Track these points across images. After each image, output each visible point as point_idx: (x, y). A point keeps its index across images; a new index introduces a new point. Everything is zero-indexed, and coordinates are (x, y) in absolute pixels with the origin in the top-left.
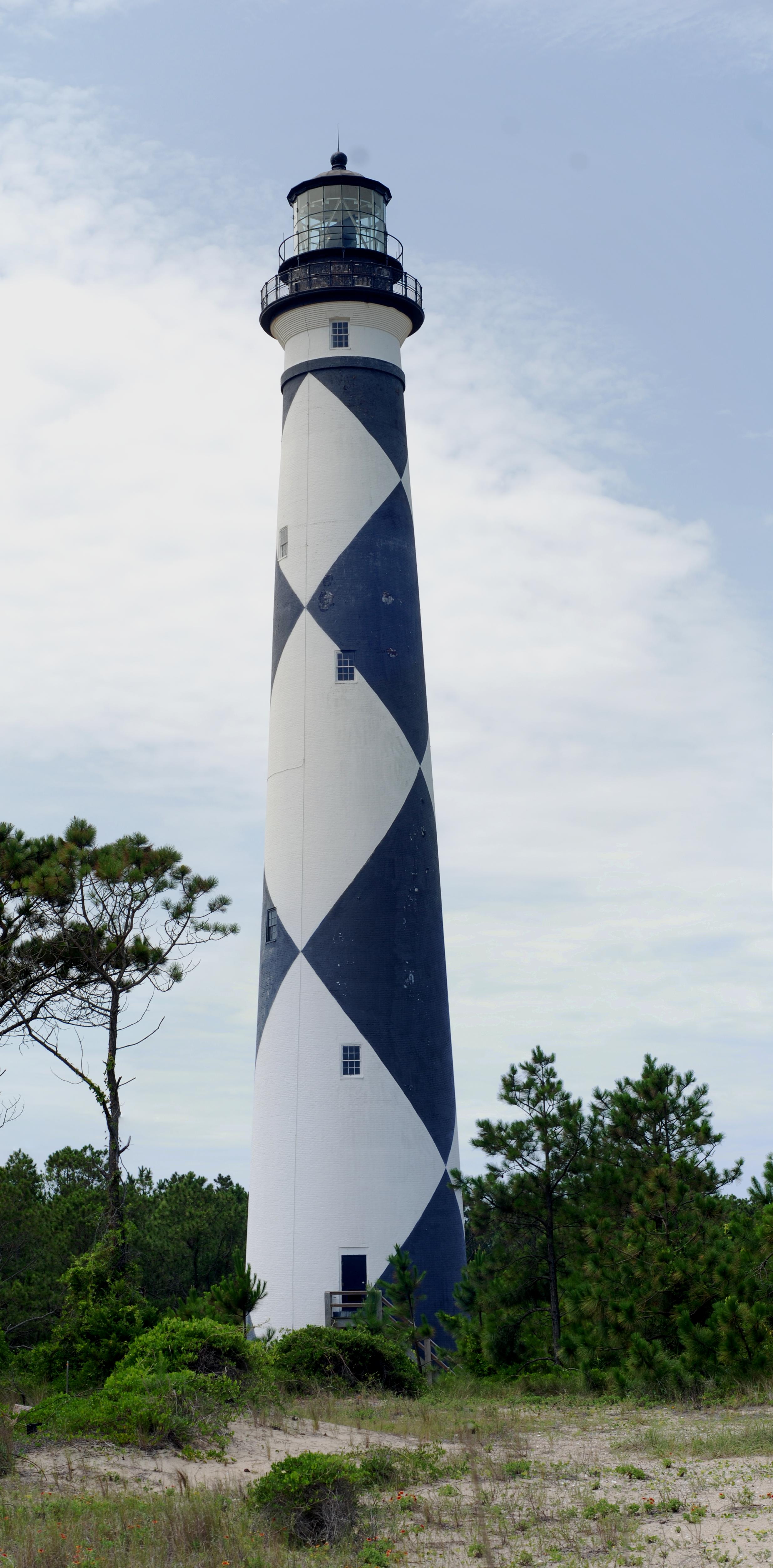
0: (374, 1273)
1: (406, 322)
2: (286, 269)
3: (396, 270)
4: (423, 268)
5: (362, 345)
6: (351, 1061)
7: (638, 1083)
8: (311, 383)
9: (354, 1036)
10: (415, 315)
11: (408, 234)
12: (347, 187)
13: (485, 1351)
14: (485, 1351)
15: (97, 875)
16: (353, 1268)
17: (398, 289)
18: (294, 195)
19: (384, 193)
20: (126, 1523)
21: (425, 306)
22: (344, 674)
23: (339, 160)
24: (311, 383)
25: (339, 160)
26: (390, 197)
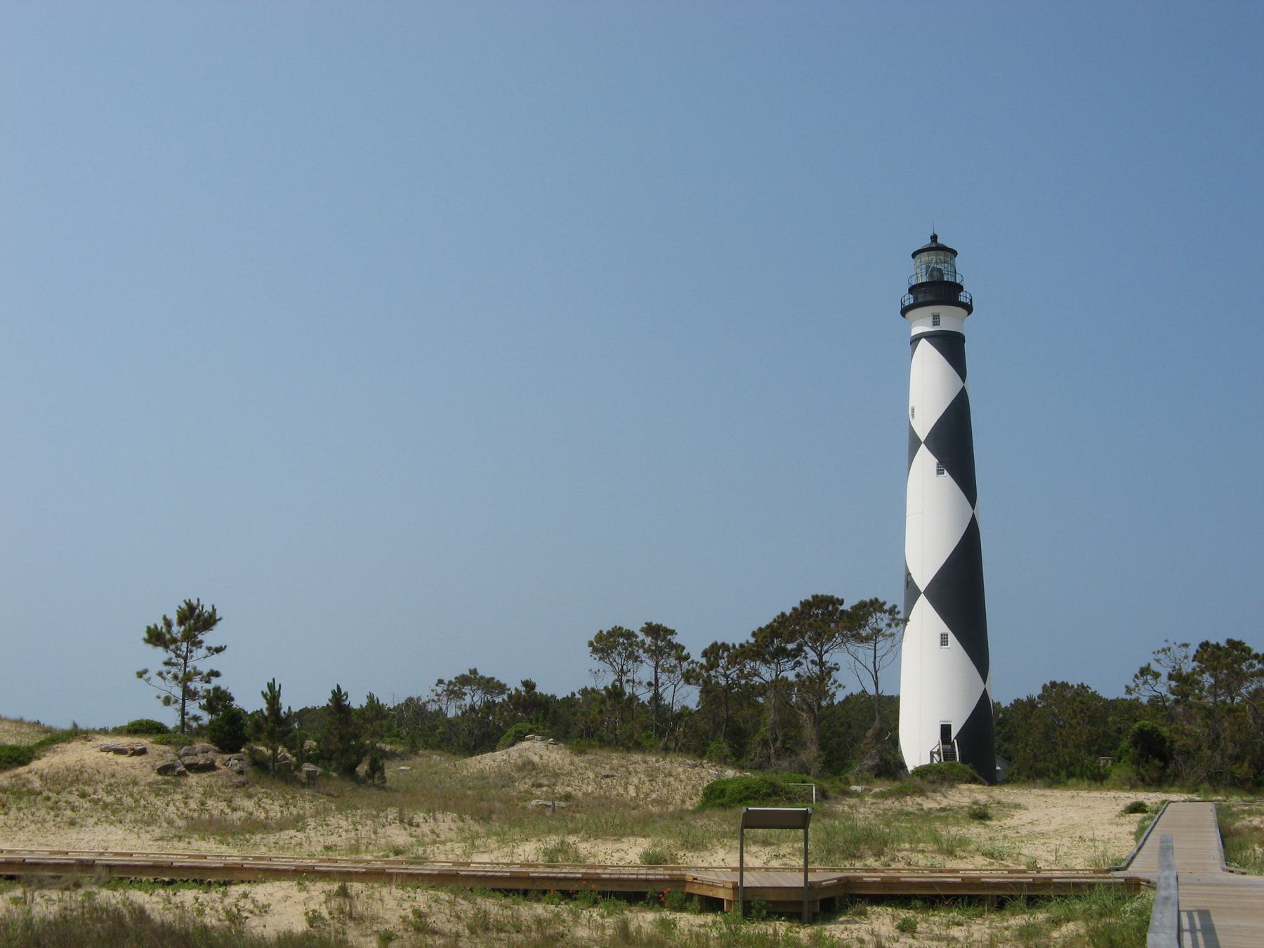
0: (954, 733)
1: (965, 312)
2: (912, 290)
3: (960, 288)
4: (971, 289)
5: (946, 325)
6: (944, 640)
7: (994, 697)
8: (924, 342)
9: (944, 628)
10: (968, 308)
11: (965, 271)
12: (936, 247)
13: (1137, 725)
14: (1137, 725)
15: (1079, 936)
16: (946, 730)
17: (962, 299)
18: (914, 255)
19: (954, 253)
20: (762, 938)
22: (939, 472)
23: (934, 238)
24: (924, 342)
25: (934, 238)
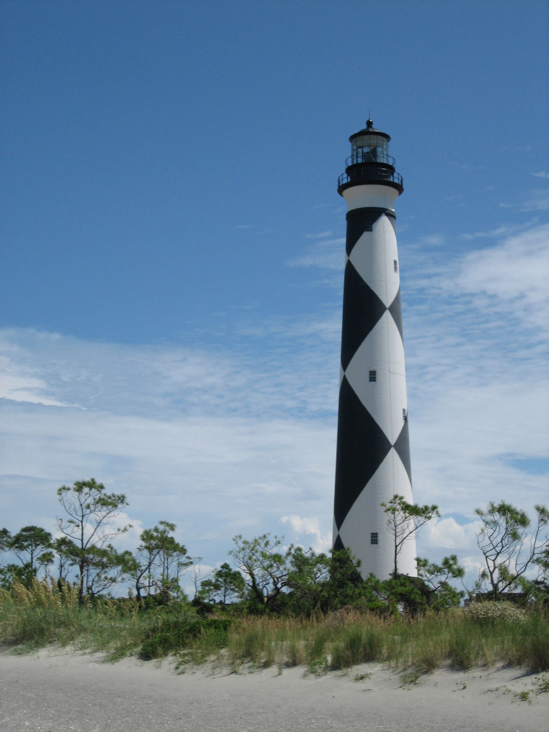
18: (353, 138)
19: (387, 137)
21: (404, 186)
23: (369, 124)
25: (369, 124)
26: (390, 138)
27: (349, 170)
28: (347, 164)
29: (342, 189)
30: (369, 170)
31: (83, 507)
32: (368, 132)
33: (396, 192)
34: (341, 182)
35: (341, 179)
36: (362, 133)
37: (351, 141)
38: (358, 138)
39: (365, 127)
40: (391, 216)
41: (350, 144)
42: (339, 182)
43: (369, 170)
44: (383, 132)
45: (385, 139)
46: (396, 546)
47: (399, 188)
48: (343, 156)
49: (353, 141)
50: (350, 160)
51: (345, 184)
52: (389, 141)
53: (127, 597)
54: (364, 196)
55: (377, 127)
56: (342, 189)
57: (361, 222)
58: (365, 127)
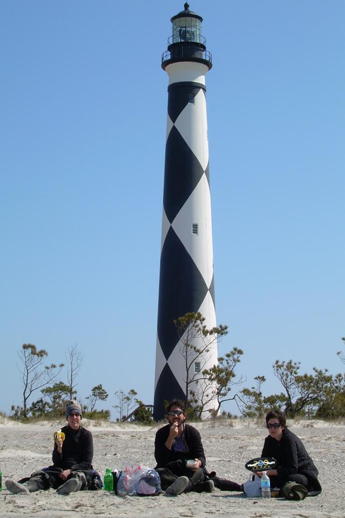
18: (173, 19)
19: (200, 19)
23: (186, 6)
25: (186, 6)
26: (202, 20)
27: (170, 48)
28: (168, 42)
29: (165, 64)
30: (185, 50)
31: (204, 395)
32: (186, 14)
33: (206, 67)
34: (165, 59)
35: (165, 55)
36: (181, 15)
37: (172, 22)
38: (146, 493)
39: (183, 9)
40: (204, 90)
41: (171, 25)
42: (163, 58)
43: (185, 50)
44: (197, 14)
45: (198, 20)
46: (25, 400)
47: (208, 64)
48: (166, 36)
49: (174, 21)
50: (171, 38)
51: (168, 60)
52: (201, 21)
53: (149, 433)
54: (184, 71)
55: (192, 9)
56: (165, 64)
57: (181, 96)
58: (183, 9)
